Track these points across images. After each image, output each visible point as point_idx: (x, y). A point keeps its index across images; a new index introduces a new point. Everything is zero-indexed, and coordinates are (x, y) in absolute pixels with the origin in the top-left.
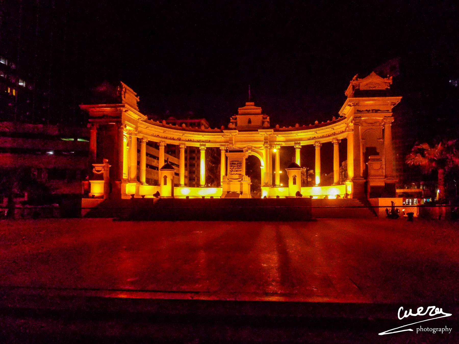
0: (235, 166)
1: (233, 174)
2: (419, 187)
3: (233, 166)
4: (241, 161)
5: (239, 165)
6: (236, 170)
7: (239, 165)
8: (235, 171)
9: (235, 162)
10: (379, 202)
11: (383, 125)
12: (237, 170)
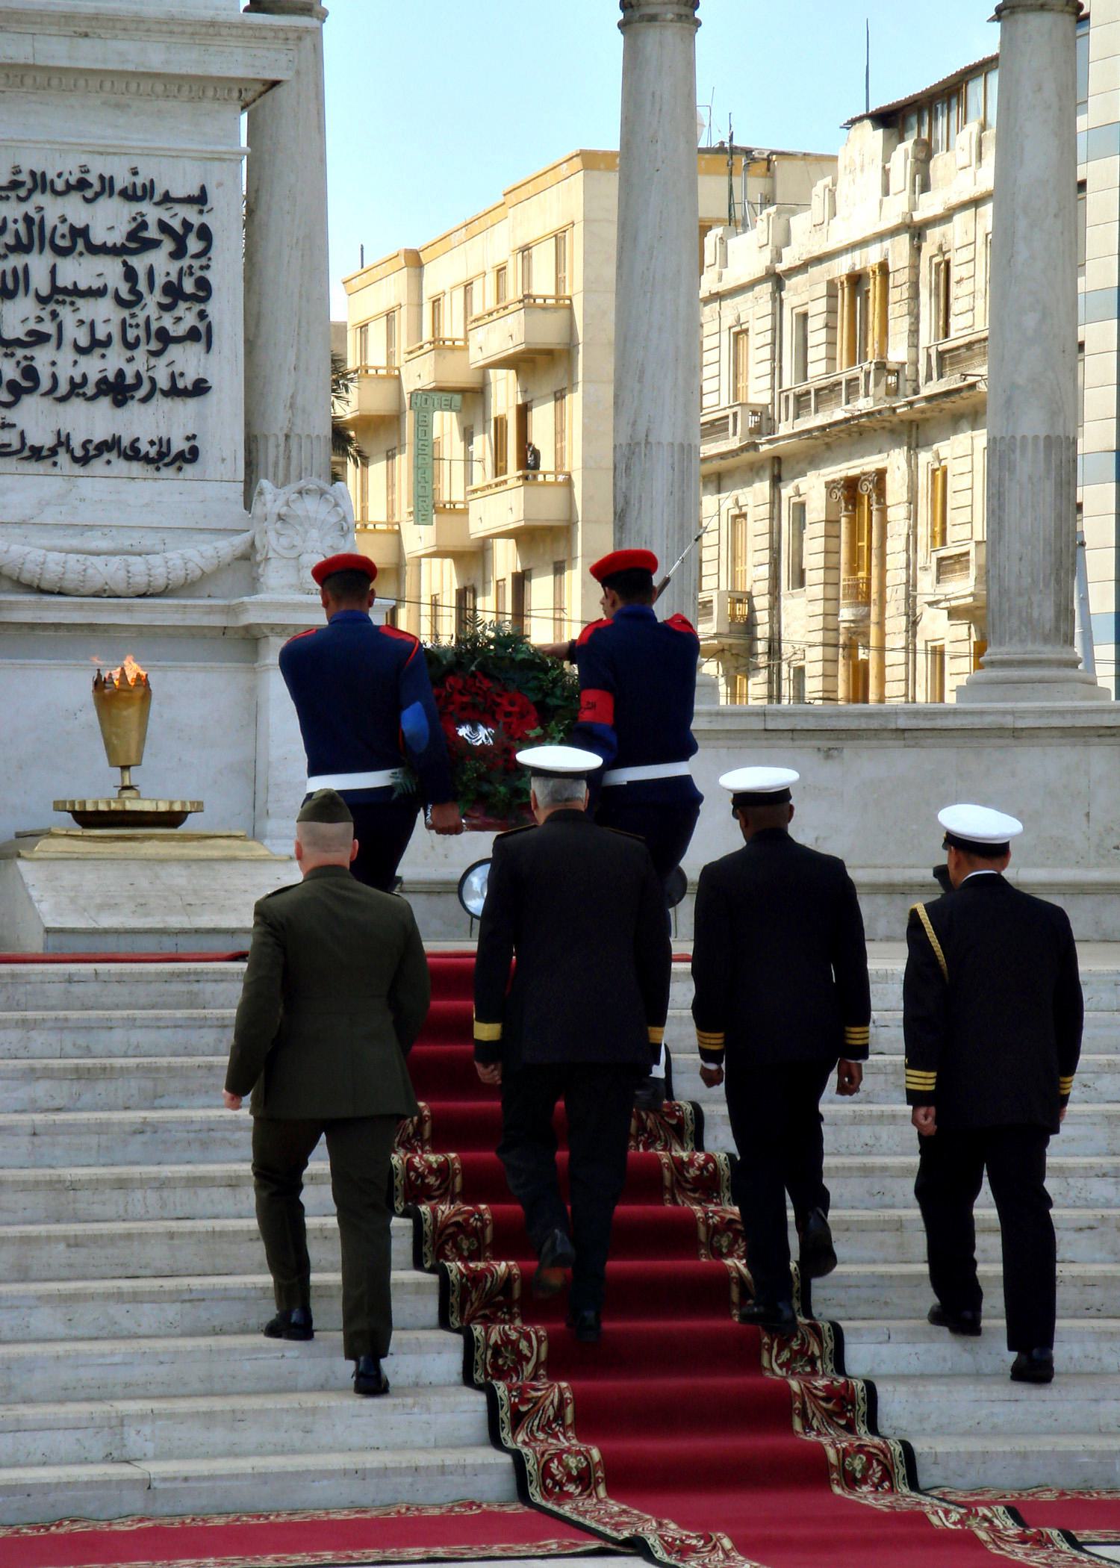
0: (76, 292)
1: (36, 454)
2: (410, 1166)
3: (40, 281)
4: (200, 199)
5: (160, 262)
6: (93, 367)
7: (160, 262)
8: (76, 388)
9: (74, 210)
10: (242, 284)
11: (554, 1486)
12: (113, 362)
